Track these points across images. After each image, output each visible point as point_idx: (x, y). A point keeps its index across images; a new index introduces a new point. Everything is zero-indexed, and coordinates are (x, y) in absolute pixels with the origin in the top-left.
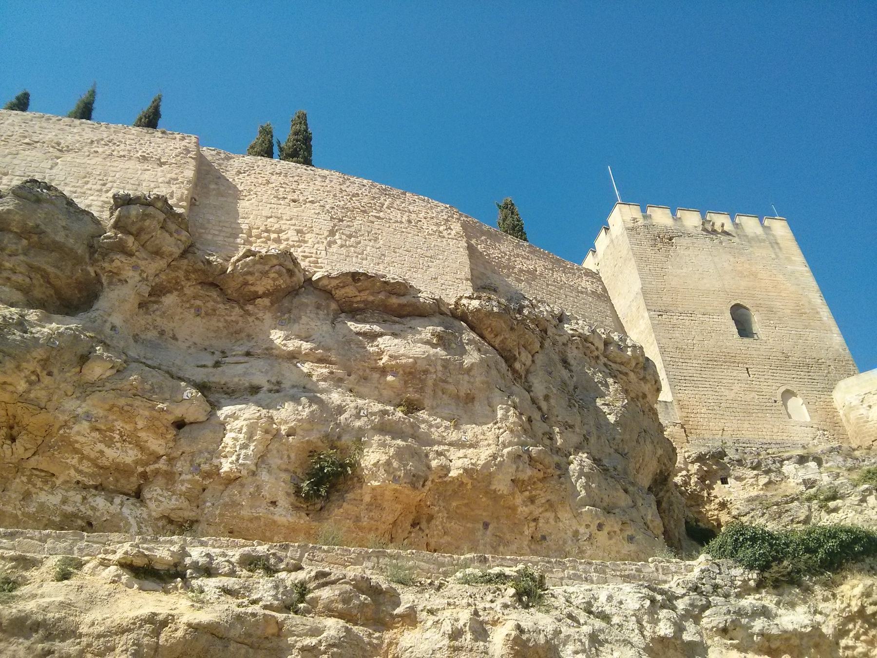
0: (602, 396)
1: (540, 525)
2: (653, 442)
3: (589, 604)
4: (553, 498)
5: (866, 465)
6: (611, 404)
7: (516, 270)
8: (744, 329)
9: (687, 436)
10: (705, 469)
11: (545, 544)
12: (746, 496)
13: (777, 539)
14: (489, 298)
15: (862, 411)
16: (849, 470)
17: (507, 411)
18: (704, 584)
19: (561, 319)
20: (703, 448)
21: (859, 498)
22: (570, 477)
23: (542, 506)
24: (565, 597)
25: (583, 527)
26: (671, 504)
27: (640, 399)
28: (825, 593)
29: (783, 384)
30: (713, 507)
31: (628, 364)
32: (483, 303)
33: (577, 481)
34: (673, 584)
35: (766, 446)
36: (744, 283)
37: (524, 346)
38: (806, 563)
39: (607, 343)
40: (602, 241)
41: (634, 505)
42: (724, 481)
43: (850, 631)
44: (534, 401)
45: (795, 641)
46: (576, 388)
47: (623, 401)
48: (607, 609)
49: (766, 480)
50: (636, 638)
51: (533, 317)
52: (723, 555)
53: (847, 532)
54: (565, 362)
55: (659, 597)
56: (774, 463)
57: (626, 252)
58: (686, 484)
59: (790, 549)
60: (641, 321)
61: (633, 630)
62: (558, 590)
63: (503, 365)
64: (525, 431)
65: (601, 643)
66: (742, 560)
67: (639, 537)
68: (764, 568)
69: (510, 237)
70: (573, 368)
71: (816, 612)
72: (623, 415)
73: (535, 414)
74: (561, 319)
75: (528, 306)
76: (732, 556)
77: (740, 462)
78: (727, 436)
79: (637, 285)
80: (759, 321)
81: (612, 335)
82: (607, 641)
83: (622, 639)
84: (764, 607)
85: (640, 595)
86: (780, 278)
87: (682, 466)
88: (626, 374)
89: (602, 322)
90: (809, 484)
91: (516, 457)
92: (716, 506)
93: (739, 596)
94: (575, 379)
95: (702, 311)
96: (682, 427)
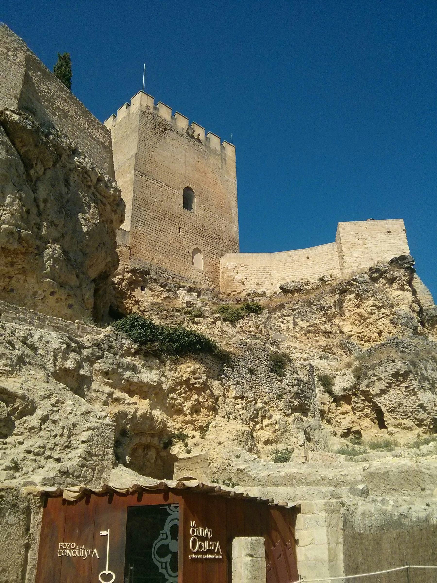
0: (84, 212)
1: (13, 281)
2: (106, 252)
3: (26, 338)
4: (27, 267)
5: (223, 304)
6: (88, 220)
7: (54, 106)
8: (187, 204)
9: (130, 255)
10: (134, 278)
11: (12, 294)
12: (152, 301)
13: (157, 329)
14: (27, 118)
15: (232, 274)
16: (213, 304)
17: (14, 200)
18: (104, 344)
19: (75, 152)
20: (137, 266)
21: (212, 320)
22: (43, 257)
23: (18, 270)
24: (11, 330)
25: (42, 291)
26: (105, 292)
27: (108, 223)
28: (172, 366)
29: (196, 244)
30: (130, 302)
31: (108, 198)
32: (22, 119)
33: (47, 261)
34: (85, 339)
35: (173, 276)
36: (197, 176)
37: (42, 161)
38: (167, 347)
39: (100, 180)
40: (122, 112)
41: (80, 287)
42: (143, 289)
43: (178, 390)
44: (35, 200)
45: (145, 389)
46: (68, 201)
47: (96, 221)
48: (37, 344)
49: (167, 295)
50: (49, 366)
51: (54, 143)
52: (122, 330)
53: (196, 336)
54: (67, 182)
55: (73, 345)
56: (175, 287)
57: (134, 126)
58: (120, 283)
59: (161, 337)
60: (128, 175)
61: (49, 360)
62: (8, 325)
63: (22, 168)
64: (22, 218)
65: (25, 364)
66: (132, 336)
67: (76, 306)
68: (142, 344)
69: (58, 81)
70: (71, 188)
71: (163, 375)
72: (93, 229)
73: (33, 209)
74: (75, 152)
75: (54, 134)
76: (127, 331)
77: (155, 281)
78: (153, 263)
79: (134, 151)
80: (197, 202)
81: (105, 176)
82: (29, 363)
83: (40, 364)
84: (134, 365)
85: (61, 341)
86: (219, 181)
87: (121, 272)
88: (105, 204)
89: (101, 165)
90: (189, 304)
91: (10, 233)
92: (133, 302)
93: (122, 356)
94: (69, 195)
95: (167, 183)
96: (130, 249)
